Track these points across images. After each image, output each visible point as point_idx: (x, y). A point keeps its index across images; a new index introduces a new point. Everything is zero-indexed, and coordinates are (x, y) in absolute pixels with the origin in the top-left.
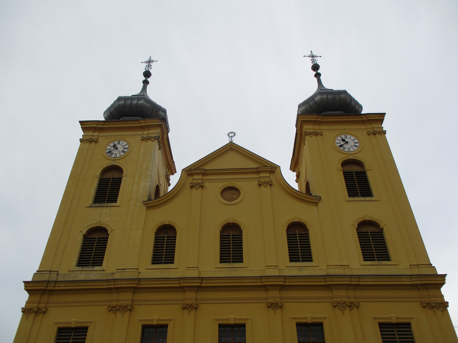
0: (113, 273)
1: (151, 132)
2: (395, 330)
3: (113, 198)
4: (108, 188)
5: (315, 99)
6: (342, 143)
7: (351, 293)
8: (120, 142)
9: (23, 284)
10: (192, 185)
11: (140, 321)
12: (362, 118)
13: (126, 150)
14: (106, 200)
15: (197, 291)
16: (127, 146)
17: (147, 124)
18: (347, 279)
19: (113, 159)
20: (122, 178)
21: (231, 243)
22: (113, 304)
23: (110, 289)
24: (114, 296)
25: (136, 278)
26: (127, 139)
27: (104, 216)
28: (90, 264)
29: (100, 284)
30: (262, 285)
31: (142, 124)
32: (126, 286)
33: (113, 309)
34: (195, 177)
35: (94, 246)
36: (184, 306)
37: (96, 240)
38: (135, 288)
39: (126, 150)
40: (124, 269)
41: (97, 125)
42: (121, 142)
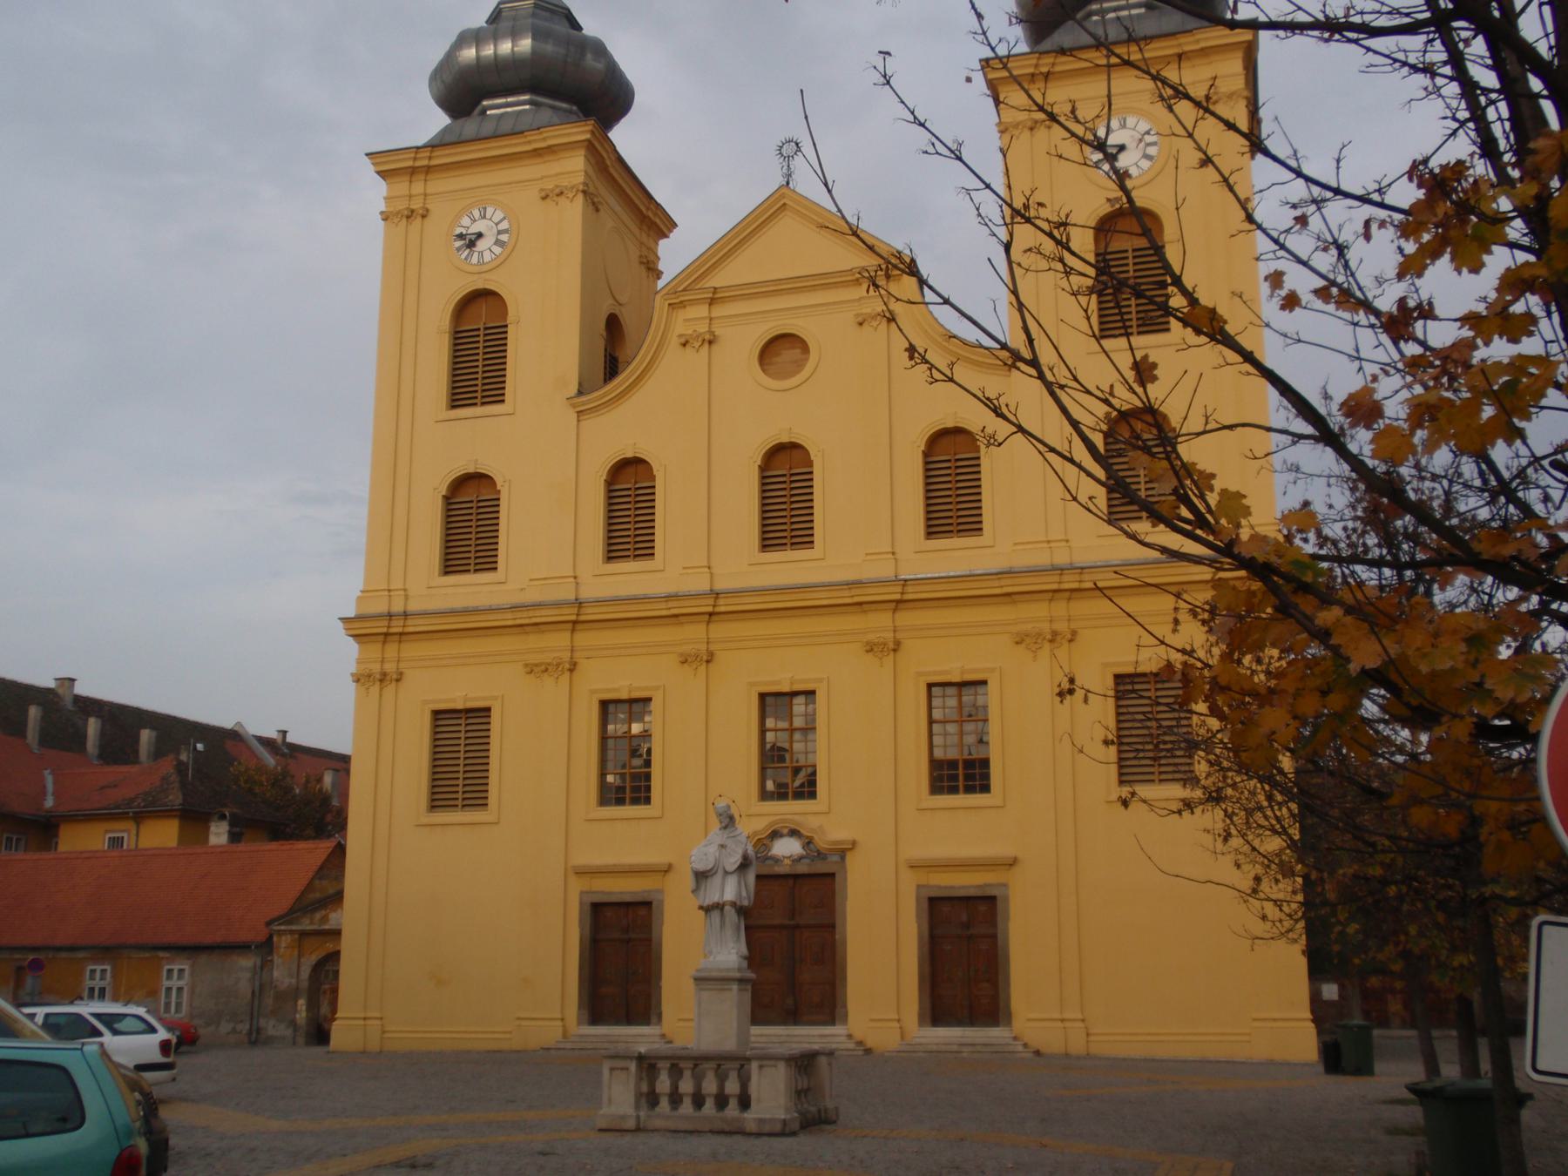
3: (476, 797)
4: (476, 357)
7: (1060, 608)
9: (340, 624)
11: (593, 692)
13: (504, 237)
15: (895, 610)
16: (504, 225)
19: (477, 269)
21: (786, 492)
24: (534, 641)
27: (477, 440)
29: (500, 616)
30: (852, 600)
35: (469, 520)
38: (711, 614)
39: (504, 237)
41: (415, 159)
42: (490, 211)
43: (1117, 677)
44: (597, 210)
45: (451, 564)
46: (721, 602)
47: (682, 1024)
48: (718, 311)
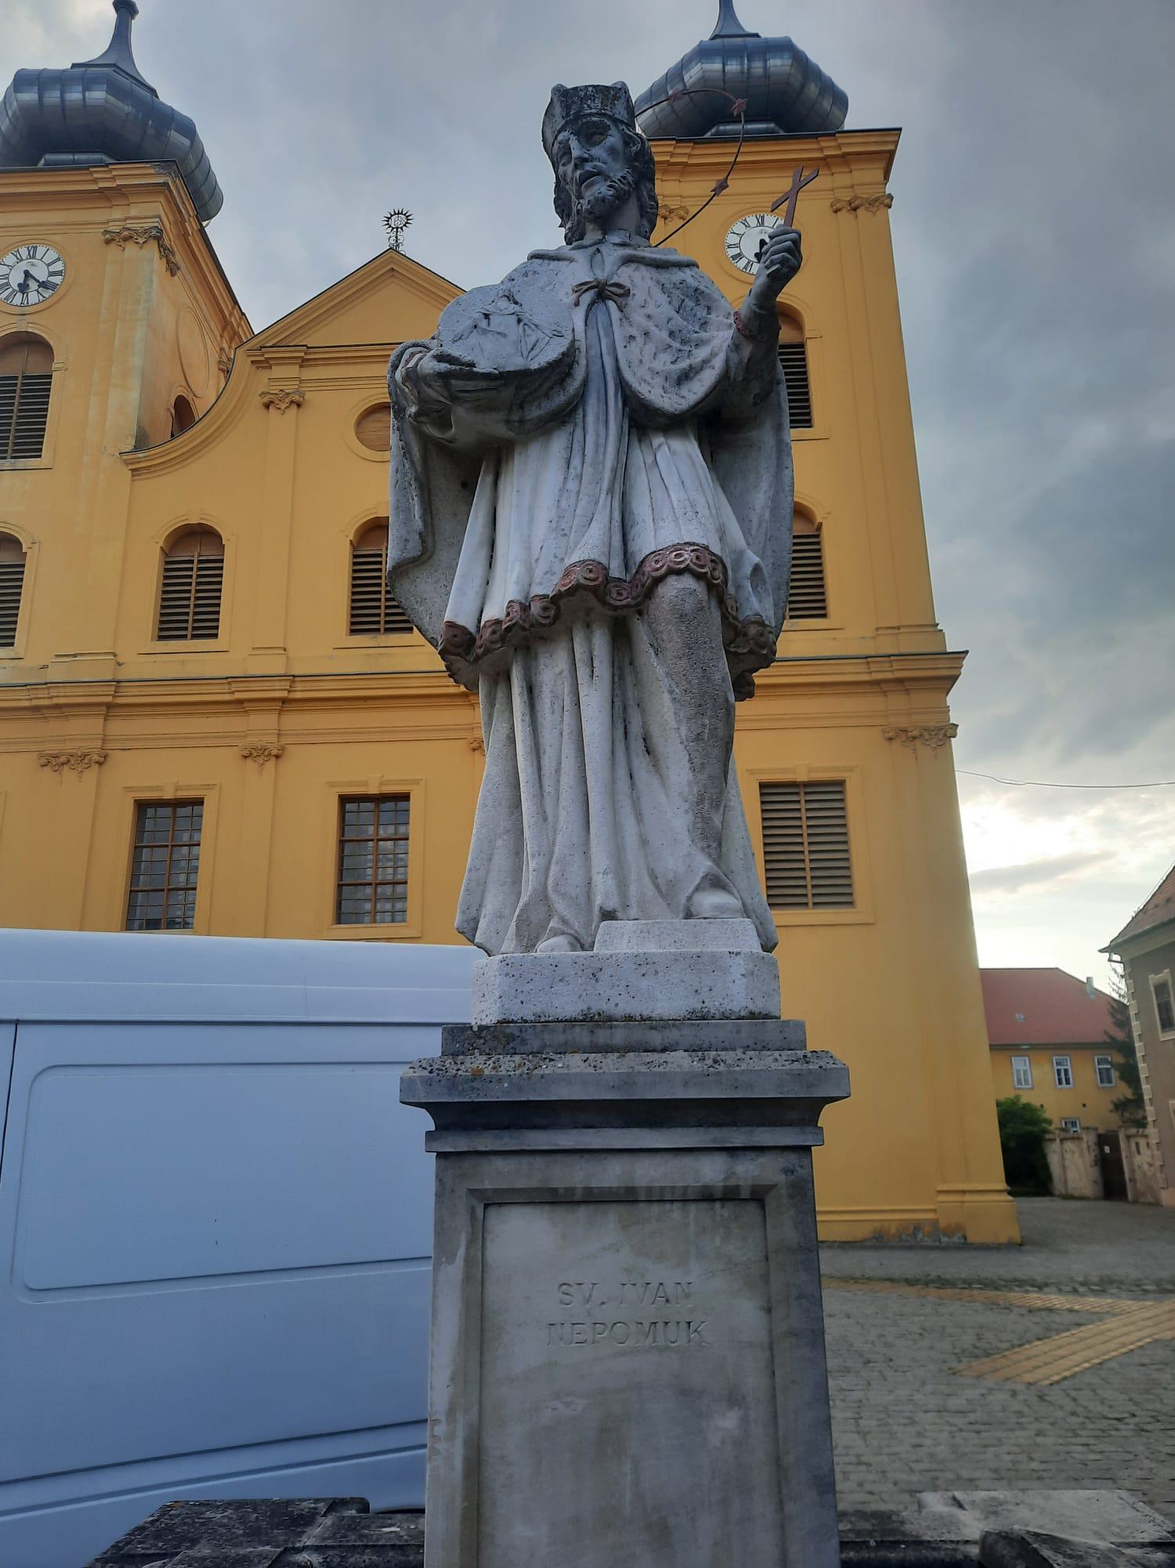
0: (45, 667)
1: (134, 211)
2: (803, 798)
5: (686, 78)
6: (33, 285)
8: (35, 248)
10: (266, 399)
12: (821, 149)
13: (57, 280)
14: (10, 448)
15: (280, 712)
16: (59, 266)
17: (119, 182)
18: (277, 685)
20: (50, 377)
22: (52, 748)
23: (36, 709)
24: (54, 727)
25: (282, 672)
26: (57, 238)
28: (189, 633)
31: (102, 185)
32: (81, 700)
33: (54, 762)
34: (278, 371)
36: (245, 753)
37: (195, 566)
38: (284, 701)
39: (57, 280)
40: (75, 656)
42: (41, 250)
43: (762, 786)
44: (173, 275)
45: (170, 627)
46: (299, 686)
47: (942, 1198)
48: (309, 373)
